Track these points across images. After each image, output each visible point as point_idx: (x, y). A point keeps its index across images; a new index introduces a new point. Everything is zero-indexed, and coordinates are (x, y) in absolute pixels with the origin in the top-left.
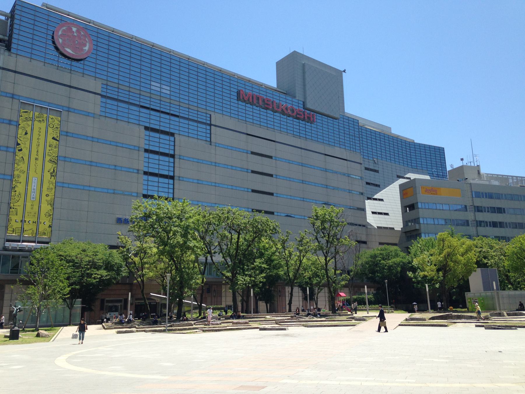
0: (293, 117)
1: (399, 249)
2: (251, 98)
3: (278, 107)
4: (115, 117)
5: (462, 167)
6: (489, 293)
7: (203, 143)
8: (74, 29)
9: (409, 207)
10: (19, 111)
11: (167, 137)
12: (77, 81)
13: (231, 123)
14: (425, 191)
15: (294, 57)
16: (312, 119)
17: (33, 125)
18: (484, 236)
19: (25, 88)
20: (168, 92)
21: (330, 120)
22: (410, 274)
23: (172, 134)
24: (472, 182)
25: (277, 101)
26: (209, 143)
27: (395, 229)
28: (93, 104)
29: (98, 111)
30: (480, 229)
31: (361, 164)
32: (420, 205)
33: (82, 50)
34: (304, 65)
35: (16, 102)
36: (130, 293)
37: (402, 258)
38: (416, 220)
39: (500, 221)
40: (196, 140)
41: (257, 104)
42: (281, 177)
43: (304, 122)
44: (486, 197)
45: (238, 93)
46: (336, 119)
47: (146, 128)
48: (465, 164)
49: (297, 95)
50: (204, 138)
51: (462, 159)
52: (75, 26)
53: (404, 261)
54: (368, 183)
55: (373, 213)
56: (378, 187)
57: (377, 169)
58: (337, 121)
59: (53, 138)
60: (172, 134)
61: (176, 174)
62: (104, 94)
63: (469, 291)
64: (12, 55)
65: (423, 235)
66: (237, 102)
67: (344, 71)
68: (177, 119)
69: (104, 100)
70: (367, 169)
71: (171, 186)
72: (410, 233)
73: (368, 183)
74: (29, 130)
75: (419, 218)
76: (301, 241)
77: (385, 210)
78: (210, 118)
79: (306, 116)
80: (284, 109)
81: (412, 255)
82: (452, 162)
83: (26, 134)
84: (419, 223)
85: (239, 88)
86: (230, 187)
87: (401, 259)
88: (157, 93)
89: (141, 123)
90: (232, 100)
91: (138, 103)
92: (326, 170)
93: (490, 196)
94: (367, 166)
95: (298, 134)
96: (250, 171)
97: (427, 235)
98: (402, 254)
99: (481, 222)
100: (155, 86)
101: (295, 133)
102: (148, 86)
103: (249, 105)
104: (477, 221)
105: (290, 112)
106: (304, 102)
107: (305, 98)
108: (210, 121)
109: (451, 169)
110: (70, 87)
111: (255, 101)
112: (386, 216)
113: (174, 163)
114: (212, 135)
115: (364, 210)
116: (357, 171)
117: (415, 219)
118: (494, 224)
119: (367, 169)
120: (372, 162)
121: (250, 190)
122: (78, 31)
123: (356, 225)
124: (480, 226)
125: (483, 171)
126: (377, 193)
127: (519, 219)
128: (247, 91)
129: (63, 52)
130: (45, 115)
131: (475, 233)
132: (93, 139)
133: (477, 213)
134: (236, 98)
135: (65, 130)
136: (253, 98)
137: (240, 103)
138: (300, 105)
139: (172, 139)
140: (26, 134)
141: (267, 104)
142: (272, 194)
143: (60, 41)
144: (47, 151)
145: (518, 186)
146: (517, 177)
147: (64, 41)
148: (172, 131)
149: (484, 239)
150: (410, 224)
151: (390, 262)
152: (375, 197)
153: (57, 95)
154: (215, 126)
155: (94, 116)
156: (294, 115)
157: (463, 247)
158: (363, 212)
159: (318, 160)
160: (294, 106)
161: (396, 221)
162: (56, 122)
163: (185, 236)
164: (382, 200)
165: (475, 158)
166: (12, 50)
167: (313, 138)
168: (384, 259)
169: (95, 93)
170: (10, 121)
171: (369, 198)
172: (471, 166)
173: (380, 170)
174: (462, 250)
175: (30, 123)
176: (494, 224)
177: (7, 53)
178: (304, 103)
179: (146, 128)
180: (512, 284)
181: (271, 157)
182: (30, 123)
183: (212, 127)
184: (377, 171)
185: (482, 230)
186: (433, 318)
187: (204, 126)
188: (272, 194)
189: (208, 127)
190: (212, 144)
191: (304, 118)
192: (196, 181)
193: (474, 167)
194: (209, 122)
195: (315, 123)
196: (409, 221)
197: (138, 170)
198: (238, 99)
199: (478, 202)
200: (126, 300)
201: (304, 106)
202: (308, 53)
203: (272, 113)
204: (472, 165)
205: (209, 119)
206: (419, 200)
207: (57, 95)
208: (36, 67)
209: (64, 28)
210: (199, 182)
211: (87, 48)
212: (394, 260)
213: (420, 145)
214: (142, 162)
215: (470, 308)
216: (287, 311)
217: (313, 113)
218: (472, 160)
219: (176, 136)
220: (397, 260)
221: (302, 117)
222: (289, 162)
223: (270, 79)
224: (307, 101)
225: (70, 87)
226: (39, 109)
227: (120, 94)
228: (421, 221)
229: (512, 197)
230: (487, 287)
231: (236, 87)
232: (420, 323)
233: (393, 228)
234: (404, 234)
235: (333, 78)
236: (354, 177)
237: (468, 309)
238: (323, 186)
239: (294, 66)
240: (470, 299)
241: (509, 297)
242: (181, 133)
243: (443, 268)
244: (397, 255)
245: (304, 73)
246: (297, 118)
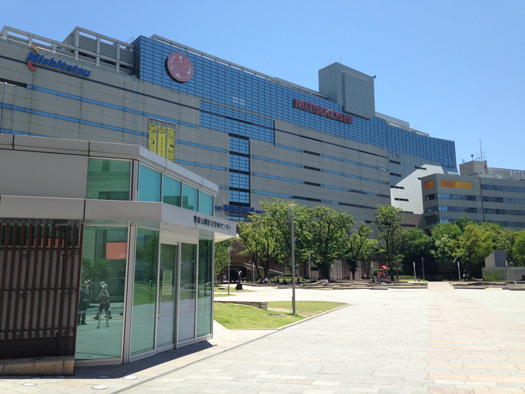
0: (335, 120)
1: (423, 232)
2: (304, 105)
3: (324, 112)
4: (209, 126)
5: (473, 161)
6: (500, 268)
7: (269, 144)
8: (181, 58)
9: (429, 196)
10: (148, 126)
11: (244, 141)
13: (288, 127)
14: (444, 184)
15: (336, 67)
16: (350, 120)
17: (157, 136)
18: (490, 222)
19: (152, 107)
20: (234, 98)
22: (433, 252)
23: (248, 139)
24: (481, 176)
25: (323, 107)
26: (273, 144)
27: (414, 213)
28: (194, 117)
29: (198, 122)
30: (485, 215)
31: (387, 158)
32: (439, 196)
33: (187, 74)
34: (343, 74)
35: (146, 118)
37: (425, 239)
38: (436, 208)
39: (503, 208)
40: (264, 143)
41: (308, 111)
43: (343, 124)
44: (492, 189)
45: (294, 102)
46: (368, 120)
47: (230, 135)
48: (474, 160)
49: (338, 100)
50: (270, 141)
51: (472, 156)
52: (181, 55)
53: (427, 241)
54: (392, 174)
55: (396, 199)
56: (400, 176)
57: (398, 161)
58: (369, 121)
59: (171, 146)
61: (251, 171)
62: (201, 108)
63: (485, 266)
64: (141, 81)
65: (441, 220)
66: (293, 109)
67: (375, 77)
68: (250, 126)
69: (201, 113)
70: (391, 161)
71: (248, 180)
72: (429, 219)
73: (392, 174)
74: (155, 139)
75: (438, 207)
76: (361, 228)
77: (408, 196)
79: (345, 118)
80: (328, 113)
81: (433, 237)
82: (462, 156)
83: (154, 143)
84: (438, 210)
85: (295, 98)
86: (289, 180)
87: (424, 240)
88: (236, 104)
89: (226, 130)
91: (224, 114)
92: (360, 164)
93: (495, 188)
95: (339, 134)
96: (303, 167)
97: (444, 220)
98: (425, 236)
99: (487, 209)
101: (336, 133)
102: (231, 100)
103: (301, 111)
104: (484, 209)
105: (333, 115)
106: (343, 107)
107: (344, 102)
108: (274, 126)
109: (462, 163)
110: (179, 104)
112: (406, 202)
113: (249, 162)
115: (389, 197)
116: (384, 164)
117: (434, 207)
118: (498, 212)
119: (391, 161)
120: (395, 155)
121: (303, 182)
122: (183, 59)
124: (486, 213)
125: (489, 166)
126: (399, 182)
127: (518, 208)
128: (301, 99)
129: (174, 77)
130: (165, 128)
131: (482, 219)
132: (196, 145)
133: (484, 202)
134: (292, 106)
135: (178, 139)
137: (295, 110)
139: (247, 142)
140: (154, 143)
141: (316, 110)
142: (319, 185)
143: (171, 68)
144: (168, 156)
145: (518, 180)
146: (517, 171)
148: (247, 136)
149: (490, 224)
150: (429, 210)
151: (416, 242)
152: (397, 185)
153: (170, 112)
154: (278, 130)
155: (196, 126)
156: (336, 118)
157: (481, 232)
158: (388, 199)
159: (354, 156)
160: (336, 110)
161: (416, 206)
162: (172, 133)
163: (301, 226)
164: (403, 188)
165: (483, 154)
166: (141, 77)
167: (350, 137)
168: (411, 240)
170: (143, 133)
171: (392, 187)
172: (479, 161)
173: (402, 162)
174: (483, 238)
175: (156, 134)
176: (498, 212)
177: (137, 80)
178: (343, 108)
179: (230, 135)
180: (514, 261)
181: (318, 155)
182: (156, 134)
183: (276, 131)
184: (399, 163)
185: (488, 216)
186: (469, 285)
188: (319, 185)
189: (273, 131)
192: (265, 176)
193: (482, 162)
196: (429, 208)
197: (226, 168)
198: (294, 106)
199: (486, 193)
202: (346, 62)
203: (319, 117)
204: (481, 160)
205: (273, 124)
206: (438, 192)
207: (170, 112)
208: (156, 90)
209: (174, 57)
210: (267, 176)
211: (189, 73)
212: (419, 240)
213: (434, 139)
214: (228, 161)
215: (486, 278)
216: (352, 279)
217: (350, 115)
218: (480, 157)
219: (250, 140)
220: (423, 240)
221: (342, 119)
222: (333, 158)
223: (314, 86)
225: (179, 104)
226: (160, 123)
227: (204, 106)
228: (440, 209)
229: (513, 189)
230: (498, 263)
232: (464, 287)
233: (412, 213)
234: (424, 219)
235: (366, 83)
237: (484, 279)
240: (486, 272)
241: (515, 271)
242: (254, 137)
243: (470, 250)
244: (421, 237)
245: (343, 81)
246: (338, 121)
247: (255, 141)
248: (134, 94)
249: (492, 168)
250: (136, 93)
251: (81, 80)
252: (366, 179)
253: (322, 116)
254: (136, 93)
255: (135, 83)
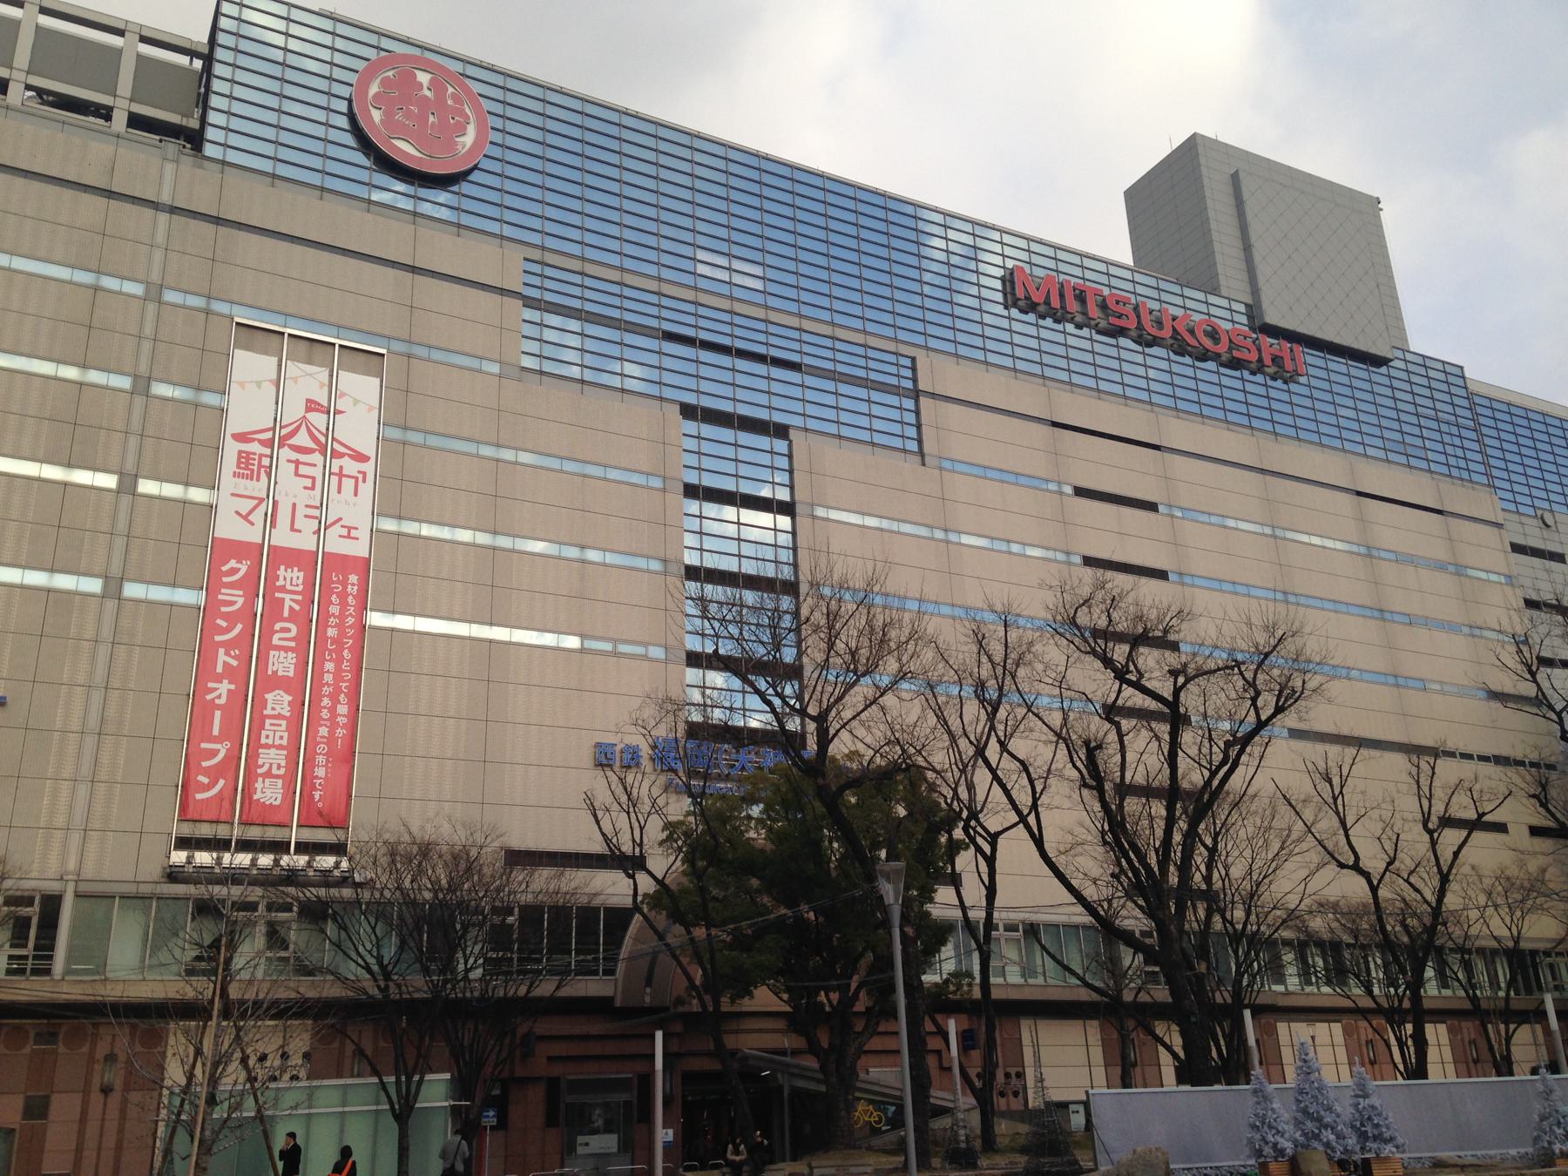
8: (423, 78)
11: (763, 442)
12: (441, 251)
16: (1289, 365)
21: (1358, 370)
23: (781, 431)
26: (918, 459)
36: (659, 1035)
42: (1197, 581)
47: (688, 411)
60: (781, 431)
61: (805, 576)
70: (1517, 548)
78: (914, 369)
79: (1269, 353)
80: (1182, 330)
89: (668, 393)
90: (987, 306)
94: (1520, 541)
100: (710, 266)
103: (1049, 322)
107: (1255, 291)
108: (915, 380)
110: (413, 269)
111: (1073, 306)
114: (801, 553)
119: (1517, 548)
120: (1535, 522)
123: (1469, 757)
134: (999, 297)
136: (1062, 296)
138: (1237, 317)
139: (781, 445)
147: (388, 116)
154: (933, 395)
166: (210, 150)
169: (502, 291)
183: (922, 399)
187: (893, 400)
189: (909, 404)
190: (927, 459)
191: (1260, 360)
194: (909, 385)
195: (1303, 380)
198: (1011, 300)
200: (647, 1080)
201: (1250, 317)
209: (390, 74)
211: (469, 139)
219: (792, 434)
221: (1254, 357)
223: (1107, 237)
224: (1265, 304)
231: (998, 260)
236: (1483, 575)
238: (1368, 613)
239: (1184, 194)
246: (1235, 364)
247: (830, 449)
248: (163, 217)
249: (266, 353)
250: (173, 210)
251: (212, 227)
252: (1411, 621)
253: (1151, 343)
254: (173, 210)
255: (169, 168)
